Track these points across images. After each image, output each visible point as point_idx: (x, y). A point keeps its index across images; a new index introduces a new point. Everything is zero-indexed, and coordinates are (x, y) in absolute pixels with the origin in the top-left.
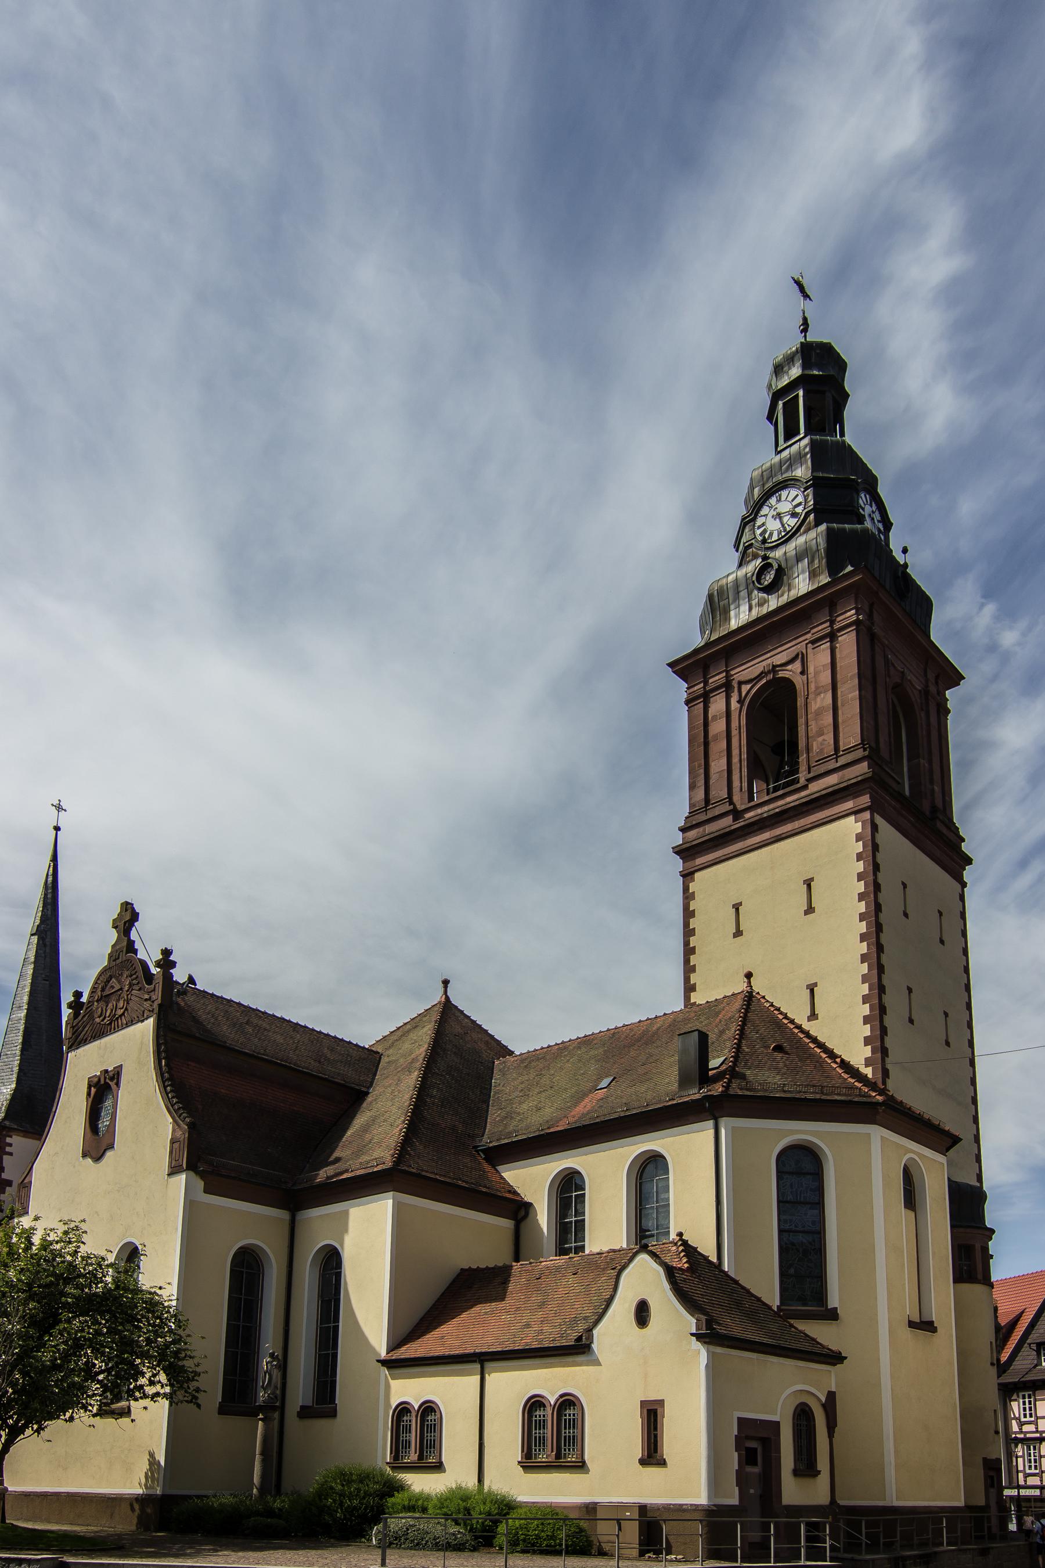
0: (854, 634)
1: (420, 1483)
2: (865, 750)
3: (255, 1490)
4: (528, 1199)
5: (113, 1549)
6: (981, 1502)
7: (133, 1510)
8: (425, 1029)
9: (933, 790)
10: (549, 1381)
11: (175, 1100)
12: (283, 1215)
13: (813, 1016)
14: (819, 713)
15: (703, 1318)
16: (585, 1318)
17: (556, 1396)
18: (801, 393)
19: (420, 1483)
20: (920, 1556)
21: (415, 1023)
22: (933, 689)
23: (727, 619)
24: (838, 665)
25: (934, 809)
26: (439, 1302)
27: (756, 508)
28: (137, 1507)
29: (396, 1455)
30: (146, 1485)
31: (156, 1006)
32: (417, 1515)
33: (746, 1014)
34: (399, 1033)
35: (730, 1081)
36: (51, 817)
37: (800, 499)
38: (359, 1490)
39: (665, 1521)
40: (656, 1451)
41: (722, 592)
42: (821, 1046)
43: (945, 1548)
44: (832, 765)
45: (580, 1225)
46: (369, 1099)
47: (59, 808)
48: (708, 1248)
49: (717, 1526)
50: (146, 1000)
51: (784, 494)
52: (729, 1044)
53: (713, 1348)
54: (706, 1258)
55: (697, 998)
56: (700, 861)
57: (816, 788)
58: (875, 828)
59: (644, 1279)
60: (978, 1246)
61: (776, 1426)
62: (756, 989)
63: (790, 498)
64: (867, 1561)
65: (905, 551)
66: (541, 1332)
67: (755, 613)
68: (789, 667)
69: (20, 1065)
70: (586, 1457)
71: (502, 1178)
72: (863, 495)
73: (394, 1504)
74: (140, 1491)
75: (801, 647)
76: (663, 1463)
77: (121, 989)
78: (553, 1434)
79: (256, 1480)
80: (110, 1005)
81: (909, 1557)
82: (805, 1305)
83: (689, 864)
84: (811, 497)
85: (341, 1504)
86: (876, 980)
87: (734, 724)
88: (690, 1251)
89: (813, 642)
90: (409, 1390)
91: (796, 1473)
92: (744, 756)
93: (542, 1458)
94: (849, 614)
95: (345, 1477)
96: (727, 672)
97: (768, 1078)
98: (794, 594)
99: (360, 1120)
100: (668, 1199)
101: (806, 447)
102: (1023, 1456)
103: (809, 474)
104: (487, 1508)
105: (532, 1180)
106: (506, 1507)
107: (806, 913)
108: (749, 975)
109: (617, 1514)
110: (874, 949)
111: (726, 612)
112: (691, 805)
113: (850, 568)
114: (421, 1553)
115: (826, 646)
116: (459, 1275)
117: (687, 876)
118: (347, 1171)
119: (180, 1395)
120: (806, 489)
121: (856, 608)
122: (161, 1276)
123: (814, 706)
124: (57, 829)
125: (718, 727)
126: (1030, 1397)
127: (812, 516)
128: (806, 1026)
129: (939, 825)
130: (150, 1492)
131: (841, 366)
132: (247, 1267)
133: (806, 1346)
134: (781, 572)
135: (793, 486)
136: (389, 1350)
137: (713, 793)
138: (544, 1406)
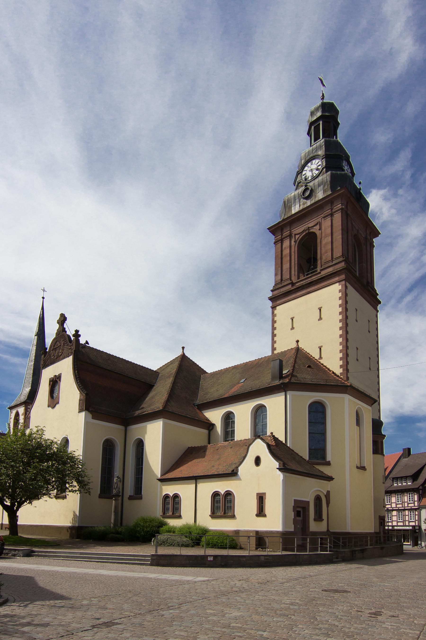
0: (340, 213)
1: (173, 523)
2: (343, 258)
3: (112, 525)
5: (55, 545)
6: (378, 531)
7: (68, 531)
8: (175, 364)
10: (221, 486)
11: (80, 385)
12: (122, 428)
13: (321, 358)
14: (326, 244)
15: (282, 463)
16: (235, 463)
17: (224, 491)
18: (321, 122)
19: (173, 523)
20: (361, 550)
21: (172, 362)
22: (369, 237)
24: (334, 226)
25: (368, 283)
26: (181, 461)
28: (69, 530)
30: (73, 523)
31: (73, 351)
32: (171, 534)
33: (296, 355)
34: (166, 366)
35: (291, 378)
36: (42, 294)
38: (150, 525)
39: (267, 537)
40: (262, 511)
41: (289, 200)
43: (369, 547)
44: (331, 264)
45: (233, 432)
46: (154, 387)
47: (44, 290)
48: (282, 438)
49: (286, 538)
51: (314, 161)
53: (285, 474)
54: (281, 442)
55: (276, 352)
56: (278, 302)
57: (324, 273)
58: (346, 287)
59: (259, 448)
60: (380, 441)
61: (308, 502)
62: (300, 346)
63: (316, 163)
64: (342, 552)
65: (360, 183)
66: (218, 468)
67: (301, 208)
68: (314, 228)
69: (32, 381)
70: (235, 514)
71: (204, 415)
72: (344, 162)
73: (163, 530)
74: (70, 525)
75: (319, 220)
76: (265, 516)
77: (60, 346)
78: (223, 505)
79: (112, 521)
80: (57, 352)
81: (357, 550)
82: (317, 460)
83: (275, 303)
84: (324, 162)
85: (143, 530)
86: (345, 344)
88: (276, 439)
89: (324, 217)
90: (170, 490)
91: (315, 520)
92: (296, 262)
93: (219, 514)
94: (339, 206)
95: (144, 520)
96: (290, 230)
97: (306, 376)
98: (317, 199)
100: (266, 422)
101: (323, 143)
102: (408, 515)
103: (324, 153)
104: (198, 532)
105: (215, 416)
106: (205, 531)
107: (319, 320)
108: (298, 341)
109: (247, 534)
110: (345, 333)
111: (290, 208)
112: (275, 281)
113: (339, 188)
114: (173, 547)
115: (329, 219)
116: (188, 449)
117: (274, 308)
118: (146, 411)
119: (82, 490)
120: (322, 159)
121: (342, 203)
122: (76, 448)
123: (324, 242)
124: (43, 298)
125: (286, 252)
126: (389, 496)
127: (325, 169)
129: (369, 288)
130: (74, 525)
131: (337, 112)
132: (109, 447)
133: (320, 474)
134: (312, 191)
135: (317, 158)
136: (162, 475)
138: (219, 495)
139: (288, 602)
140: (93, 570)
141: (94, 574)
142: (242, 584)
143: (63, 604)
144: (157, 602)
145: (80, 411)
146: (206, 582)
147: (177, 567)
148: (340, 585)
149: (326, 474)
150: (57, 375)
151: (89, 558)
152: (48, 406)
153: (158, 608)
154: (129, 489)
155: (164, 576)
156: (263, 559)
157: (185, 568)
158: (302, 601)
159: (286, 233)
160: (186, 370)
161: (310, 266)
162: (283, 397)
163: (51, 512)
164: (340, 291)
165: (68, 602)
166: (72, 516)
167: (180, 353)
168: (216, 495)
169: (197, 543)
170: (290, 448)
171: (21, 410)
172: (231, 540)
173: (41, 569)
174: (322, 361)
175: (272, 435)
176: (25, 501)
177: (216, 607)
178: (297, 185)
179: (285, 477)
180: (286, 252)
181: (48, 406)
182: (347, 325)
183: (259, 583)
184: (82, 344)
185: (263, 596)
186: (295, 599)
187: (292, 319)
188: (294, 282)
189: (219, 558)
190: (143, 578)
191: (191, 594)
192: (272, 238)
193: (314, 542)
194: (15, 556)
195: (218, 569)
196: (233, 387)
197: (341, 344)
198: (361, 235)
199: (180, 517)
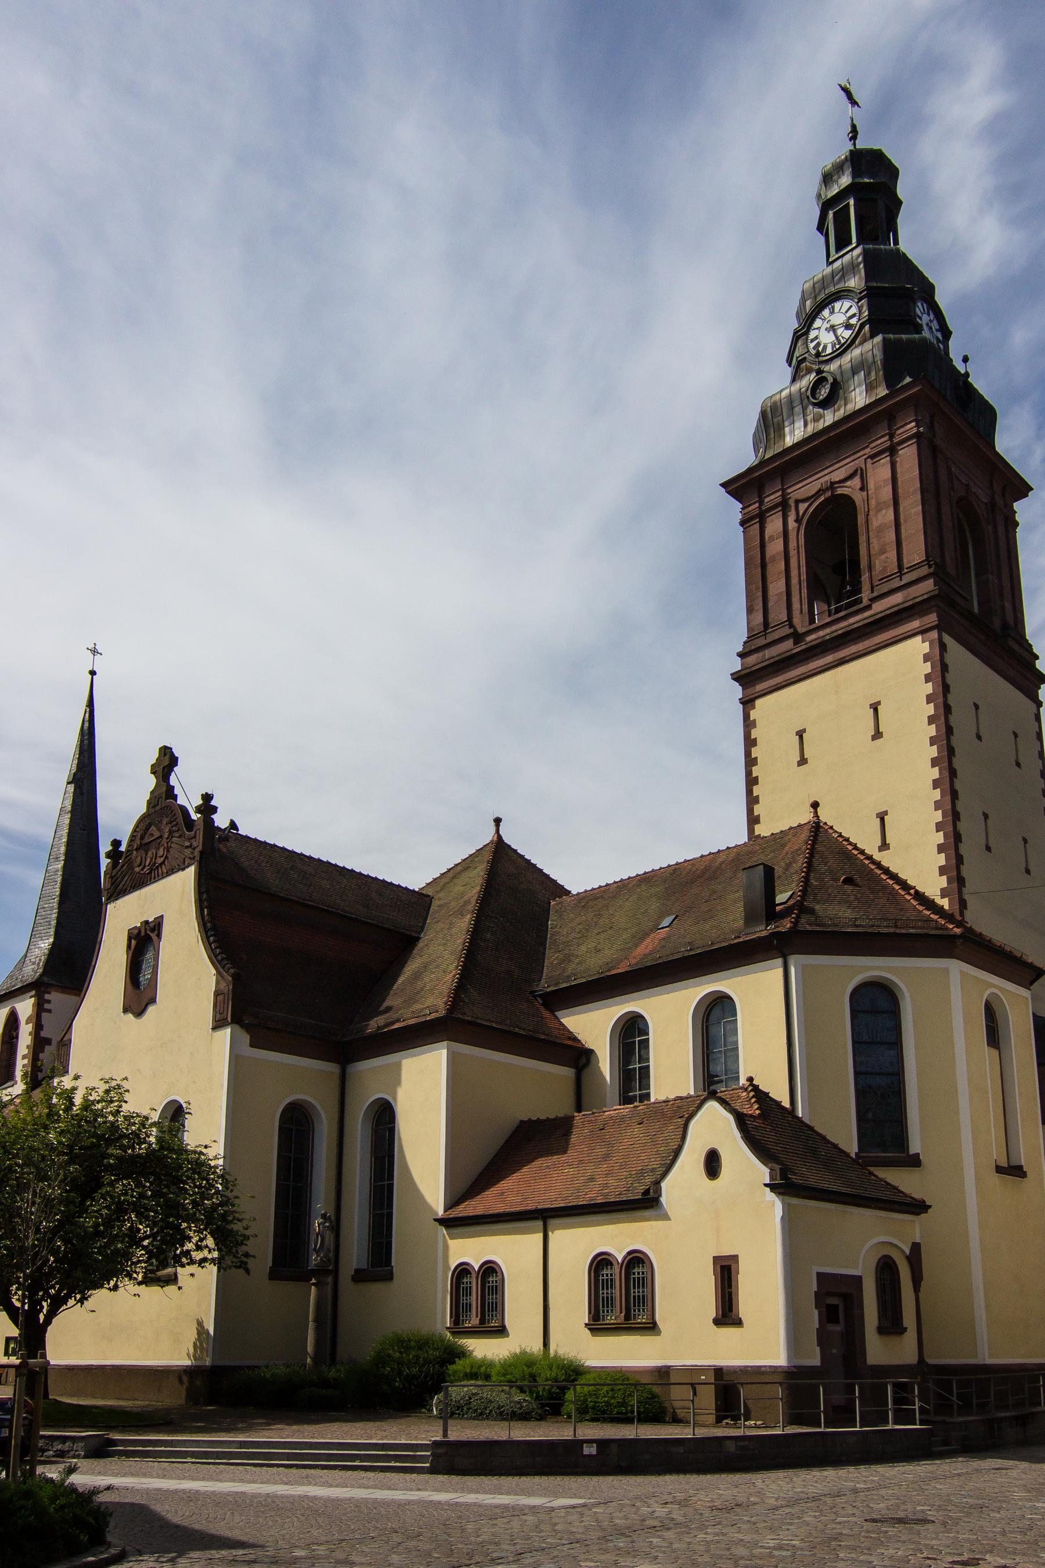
0: (915, 446)
1: (483, 1349)
2: (930, 567)
3: (309, 1360)
4: (589, 1044)
7: (181, 1381)
9: (1003, 607)
10: (616, 1238)
11: (218, 951)
12: (332, 1068)
13: (884, 846)
14: (881, 529)
15: (777, 1167)
16: (653, 1170)
17: (624, 1253)
18: (852, 202)
19: (483, 1349)
20: (1016, 1418)
23: (783, 436)
24: (900, 480)
25: (1005, 626)
26: (496, 1159)
27: (807, 321)
28: (185, 1379)
29: (456, 1319)
30: (194, 1356)
31: (197, 853)
34: (450, 875)
36: (87, 662)
37: (854, 310)
38: (417, 1357)
40: (731, 1309)
42: (894, 877)
44: (896, 583)
45: (645, 1072)
46: (421, 944)
47: (94, 651)
49: (796, 1382)
50: (187, 847)
51: (837, 305)
52: (795, 877)
53: (795, 1201)
54: (778, 1104)
56: (760, 687)
57: (879, 607)
58: (943, 647)
59: (714, 1126)
63: (844, 310)
65: (965, 360)
66: (606, 1186)
67: (810, 429)
68: (848, 483)
69: (58, 918)
71: (562, 1024)
72: (919, 304)
73: (455, 1372)
74: (188, 1363)
75: (860, 463)
76: (738, 1323)
77: (161, 837)
78: (622, 1294)
79: (310, 1349)
80: (150, 853)
83: (750, 691)
84: (865, 308)
85: (400, 1372)
87: (792, 544)
88: (761, 1097)
89: (872, 457)
90: (469, 1250)
91: (881, 1331)
92: (804, 577)
95: (402, 1343)
96: (783, 490)
97: (839, 913)
98: (850, 408)
99: (411, 967)
100: (736, 1042)
101: (858, 256)
104: (554, 1375)
105: (593, 1026)
106: (573, 1372)
108: (815, 805)
110: (946, 774)
112: (750, 629)
113: (908, 380)
114: (485, 1422)
115: (886, 460)
117: (747, 703)
120: (860, 300)
122: (207, 1134)
123: (875, 523)
124: (93, 673)
125: (775, 547)
127: (867, 327)
128: (877, 856)
130: (199, 1363)
132: (296, 1123)
133: (887, 1195)
137: (772, 616)
138: (611, 1264)
139: (772, 1544)
140: (286, 1487)
141: (292, 1496)
142: (670, 1512)
143: (253, 1557)
144: (465, 1551)
145: (218, 1024)
146: (579, 1510)
147: (501, 1475)
148: (919, 1508)
149: (906, 1195)
150: (151, 920)
151: (264, 1458)
152: (125, 1010)
153: (468, 1562)
154: (355, 1252)
155: (471, 1498)
156: (731, 1447)
157: (524, 1478)
158: (806, 1542)
159: (773, 497)
160: (509, 889)
161: (844, 587)
162: (779, 972)
163: (139, 1325)
164: (926, 658)
165: (259, 1553)
166: (193, 1335)
167: (487, 836)
168: (601, 1263)
169: (550, 1407)
170: (802, 1122)
171: (25, 1007)
172: (647, 1396)
173: (150, 1486)
174: (885, 859)
175: (752, 1084)
176: (68, 1296)
177: (602, 1557)
178: (798, 367)
179: (783, 1203)
180: (775, 547)
181: (125, 1010)
182: (951, 751)
183: (712, 1508)
184: (219, 828)
185: (717, 1534)
186: (790, 1538)
187: (800, 734)
188: (801, 630)
189: (614, 1448)
190: (419, 1502)
191: (542, 1534)
192: (734, 509)
193: (875, 1397)
194: (63, 1457)
195: (611, 1478)
196: (642, 939)
197: (938, 805)
198: (973, 500)
199: (501, 1331)
